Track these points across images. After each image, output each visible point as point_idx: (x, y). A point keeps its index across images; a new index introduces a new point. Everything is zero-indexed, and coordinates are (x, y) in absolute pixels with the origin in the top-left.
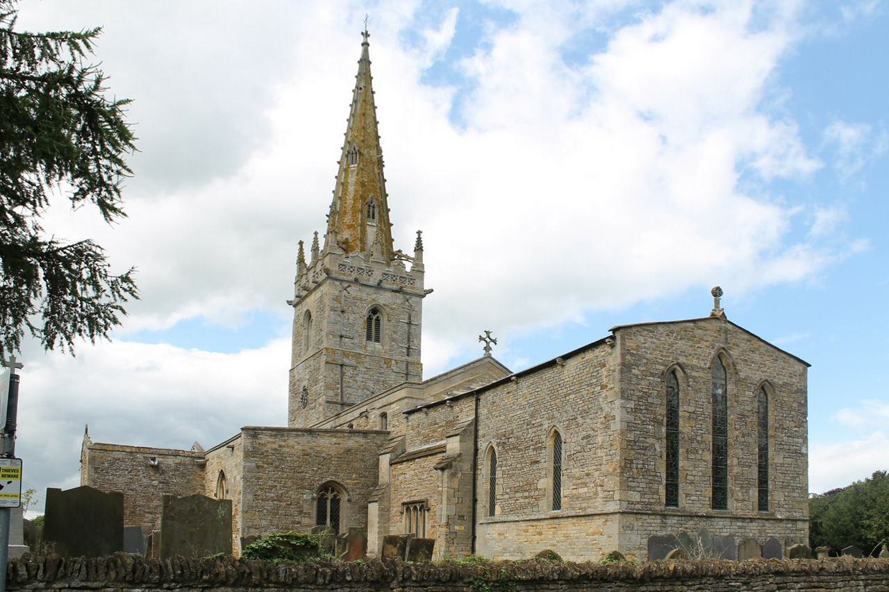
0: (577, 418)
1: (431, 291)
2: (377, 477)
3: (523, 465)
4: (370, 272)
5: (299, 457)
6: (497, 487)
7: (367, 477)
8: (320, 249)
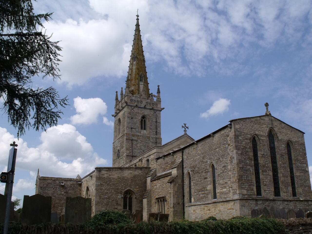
0: (220, 158)
1: (164, 109)
3: (201, 180)
4: (141, 102)
8: (123, 94)
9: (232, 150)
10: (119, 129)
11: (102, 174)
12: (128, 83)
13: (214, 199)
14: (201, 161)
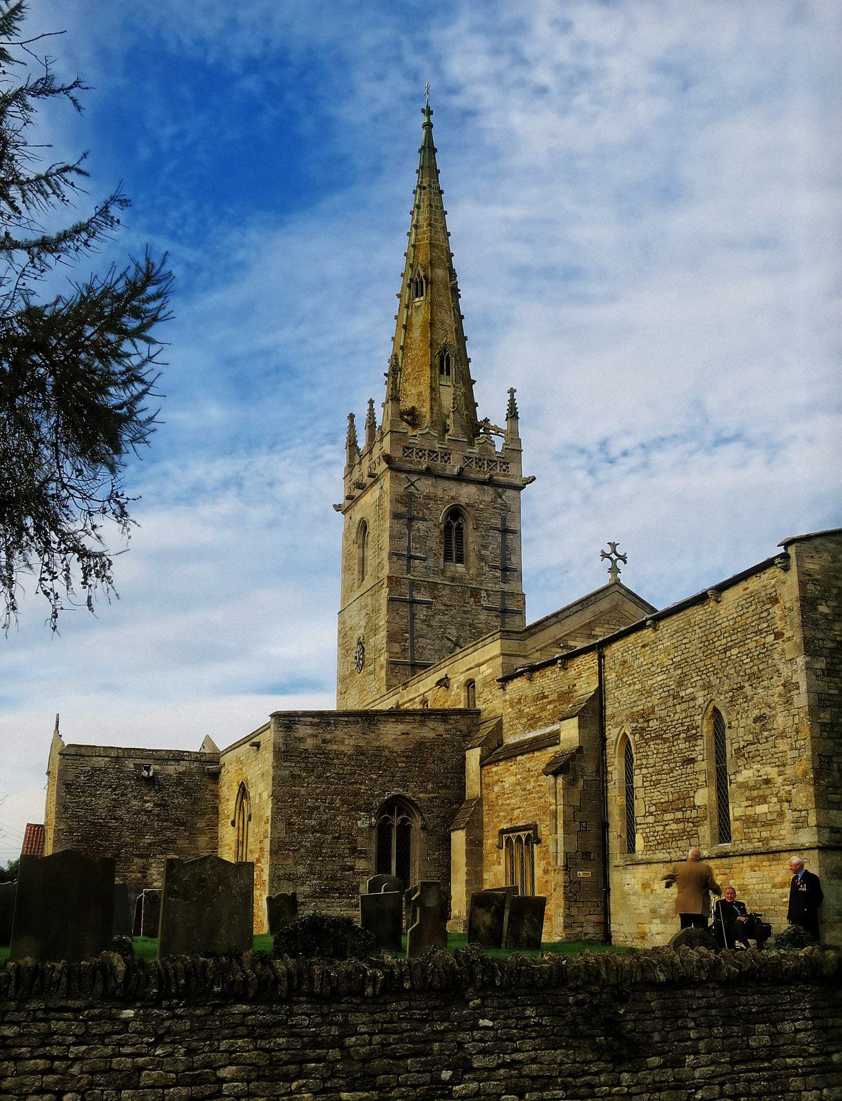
0: (744, 687)
2: (462, 786)
3: (672, 765)
4: (446, 455)
5: (350, 757)
6: (636, 802)
7: (449, 788)
8: (377, 425)
9: (791, 657)
10: (363, 561)
11: (296, 738)
12: (394, 383)
13: (721, 843)
14: (669, 696)
